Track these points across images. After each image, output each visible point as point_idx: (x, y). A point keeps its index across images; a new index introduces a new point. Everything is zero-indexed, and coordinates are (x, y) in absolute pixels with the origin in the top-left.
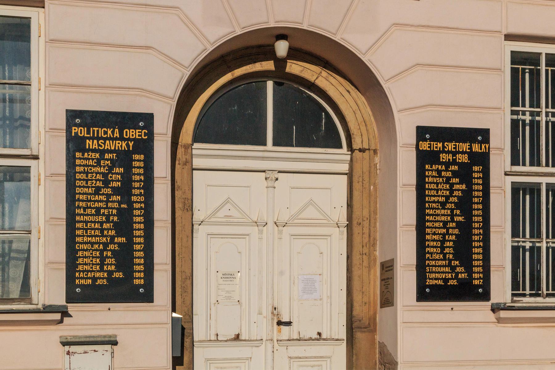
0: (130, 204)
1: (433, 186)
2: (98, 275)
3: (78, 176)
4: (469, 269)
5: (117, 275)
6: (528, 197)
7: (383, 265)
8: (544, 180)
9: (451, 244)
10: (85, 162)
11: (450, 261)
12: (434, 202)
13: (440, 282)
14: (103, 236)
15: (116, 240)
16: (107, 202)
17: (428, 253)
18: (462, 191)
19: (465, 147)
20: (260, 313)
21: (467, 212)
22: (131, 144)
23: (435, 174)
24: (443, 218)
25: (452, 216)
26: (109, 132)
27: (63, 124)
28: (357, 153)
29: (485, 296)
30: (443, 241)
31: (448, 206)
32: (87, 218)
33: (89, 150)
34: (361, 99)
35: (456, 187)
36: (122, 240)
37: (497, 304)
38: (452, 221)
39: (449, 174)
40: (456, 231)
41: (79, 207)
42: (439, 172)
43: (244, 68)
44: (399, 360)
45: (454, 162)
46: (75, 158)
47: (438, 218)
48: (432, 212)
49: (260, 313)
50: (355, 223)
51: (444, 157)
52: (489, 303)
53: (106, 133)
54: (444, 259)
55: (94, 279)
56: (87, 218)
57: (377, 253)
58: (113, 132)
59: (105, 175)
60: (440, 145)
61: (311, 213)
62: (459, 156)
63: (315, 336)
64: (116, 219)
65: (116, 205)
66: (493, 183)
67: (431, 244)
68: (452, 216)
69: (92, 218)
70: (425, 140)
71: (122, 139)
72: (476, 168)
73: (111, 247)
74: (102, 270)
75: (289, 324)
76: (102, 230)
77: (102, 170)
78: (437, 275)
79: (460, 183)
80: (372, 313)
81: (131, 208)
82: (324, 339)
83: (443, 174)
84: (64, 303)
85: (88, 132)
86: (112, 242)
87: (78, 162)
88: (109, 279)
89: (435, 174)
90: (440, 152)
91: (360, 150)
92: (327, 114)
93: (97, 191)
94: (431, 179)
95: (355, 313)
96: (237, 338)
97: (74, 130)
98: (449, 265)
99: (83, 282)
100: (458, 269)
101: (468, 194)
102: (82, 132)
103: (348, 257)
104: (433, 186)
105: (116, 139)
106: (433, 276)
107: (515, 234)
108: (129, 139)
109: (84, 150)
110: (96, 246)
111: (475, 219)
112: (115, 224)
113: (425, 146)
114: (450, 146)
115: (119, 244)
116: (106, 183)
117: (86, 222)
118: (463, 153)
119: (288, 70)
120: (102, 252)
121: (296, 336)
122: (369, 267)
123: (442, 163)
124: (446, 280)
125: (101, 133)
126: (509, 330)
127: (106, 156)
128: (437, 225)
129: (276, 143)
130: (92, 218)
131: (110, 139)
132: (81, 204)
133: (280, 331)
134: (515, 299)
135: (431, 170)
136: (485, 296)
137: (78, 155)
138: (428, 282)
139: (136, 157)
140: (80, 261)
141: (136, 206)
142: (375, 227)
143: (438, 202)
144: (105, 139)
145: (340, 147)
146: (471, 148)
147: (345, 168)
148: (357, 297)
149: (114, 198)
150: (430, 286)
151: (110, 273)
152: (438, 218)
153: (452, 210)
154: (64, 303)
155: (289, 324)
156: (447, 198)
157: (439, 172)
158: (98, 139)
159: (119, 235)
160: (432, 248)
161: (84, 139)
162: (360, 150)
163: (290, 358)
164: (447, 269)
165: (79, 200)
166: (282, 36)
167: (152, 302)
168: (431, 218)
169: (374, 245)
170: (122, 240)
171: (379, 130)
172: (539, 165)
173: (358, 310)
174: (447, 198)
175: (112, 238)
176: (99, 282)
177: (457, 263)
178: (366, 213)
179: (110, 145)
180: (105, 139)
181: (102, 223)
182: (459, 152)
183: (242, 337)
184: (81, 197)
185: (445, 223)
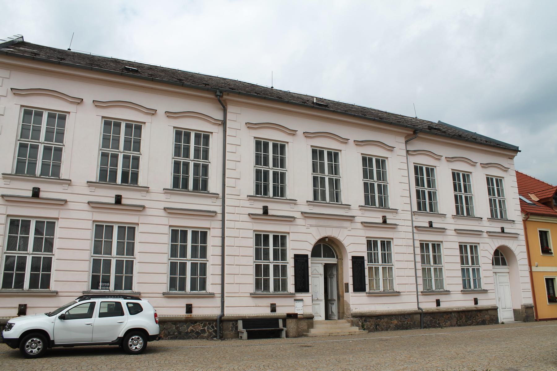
19: (360, 260)
149: (302, 271)
172: (372, 263)
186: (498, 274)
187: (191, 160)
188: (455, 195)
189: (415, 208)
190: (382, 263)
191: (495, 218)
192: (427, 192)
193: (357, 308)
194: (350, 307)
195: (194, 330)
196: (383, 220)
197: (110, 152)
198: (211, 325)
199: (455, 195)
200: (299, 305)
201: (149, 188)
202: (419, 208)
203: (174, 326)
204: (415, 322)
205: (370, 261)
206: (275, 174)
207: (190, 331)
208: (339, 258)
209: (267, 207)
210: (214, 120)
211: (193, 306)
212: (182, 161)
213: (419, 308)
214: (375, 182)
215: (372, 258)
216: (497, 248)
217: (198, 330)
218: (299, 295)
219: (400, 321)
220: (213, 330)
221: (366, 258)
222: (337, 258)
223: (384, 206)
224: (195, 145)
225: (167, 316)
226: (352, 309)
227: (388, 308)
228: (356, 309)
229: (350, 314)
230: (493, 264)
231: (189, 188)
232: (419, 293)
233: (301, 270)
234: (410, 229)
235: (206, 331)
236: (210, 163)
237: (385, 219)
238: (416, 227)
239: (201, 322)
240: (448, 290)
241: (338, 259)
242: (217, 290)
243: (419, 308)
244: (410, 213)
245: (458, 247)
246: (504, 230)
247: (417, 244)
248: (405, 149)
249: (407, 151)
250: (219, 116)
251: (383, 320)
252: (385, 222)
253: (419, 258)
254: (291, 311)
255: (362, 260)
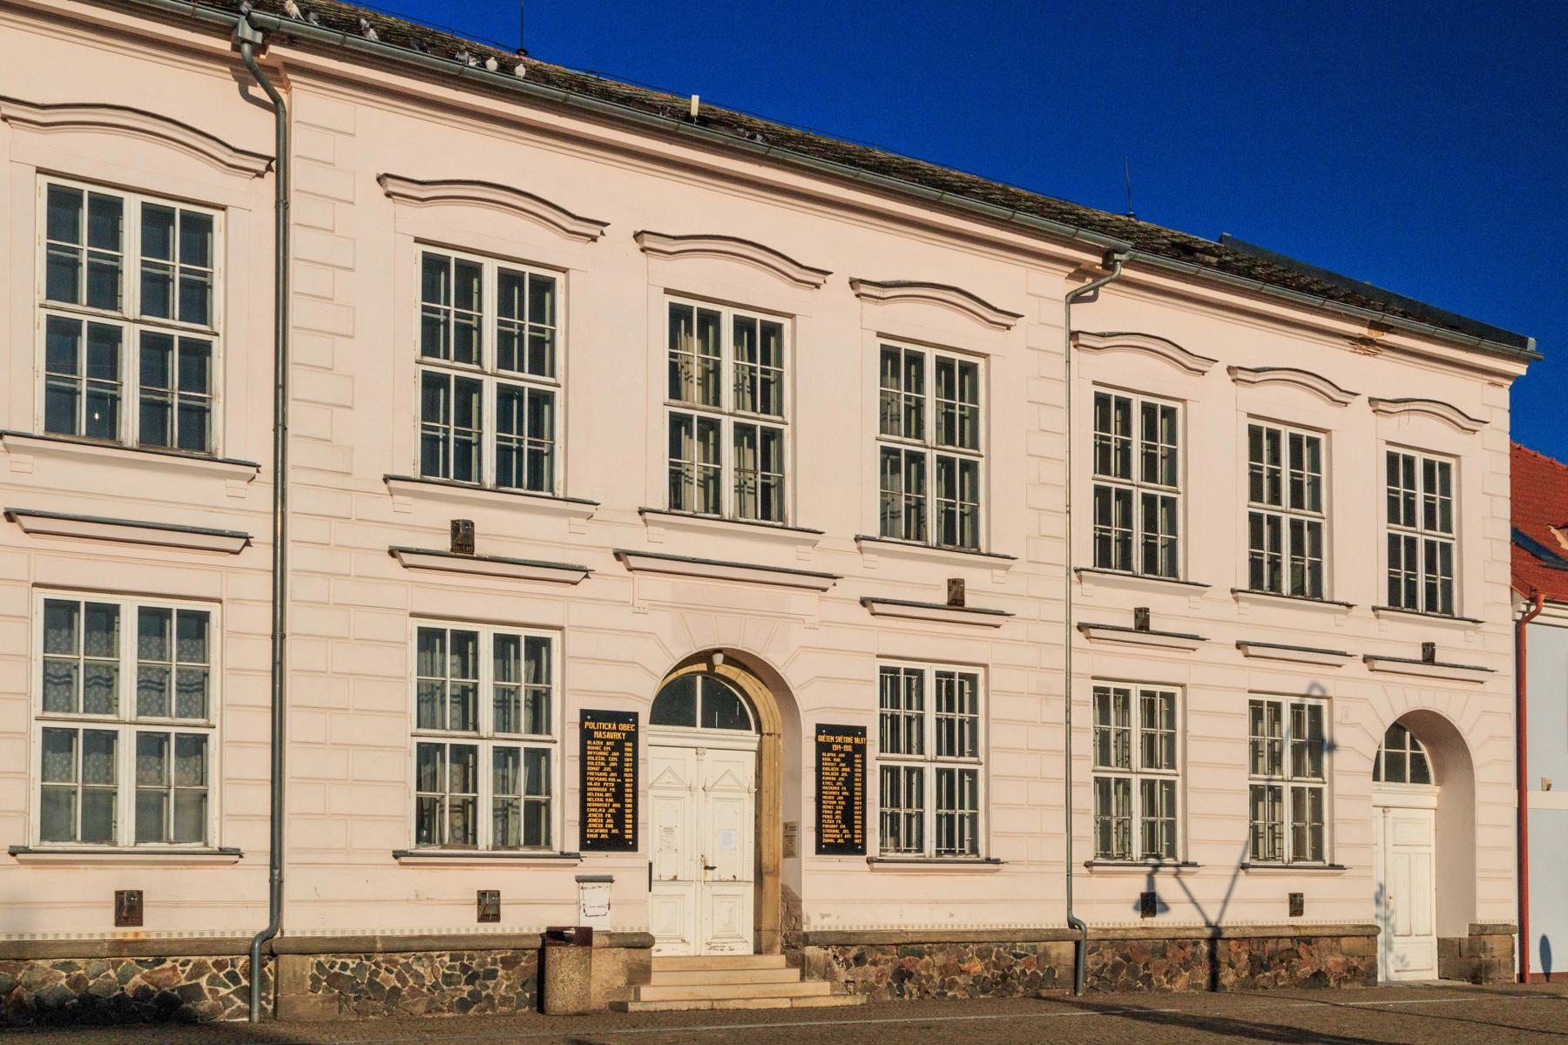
0: (623, 779)
1: (828, 769)
2: (601, 831)
3: (589, 758)
4: (852, 832)
5: (613, 831)
6: (889, 774)
7: (786, 826)
8: (453, 373)
9: (840, 812)
10: (593, 748)
11: (839, 825)
12: (828, 781)
13: (832, 841)
14: (605, 802)
15: (614, 805)
16: (608, 777)
17: (824, 818)
18: (848, 773)
19: (849, 739)
20: (692, 860)
21: (851, 790)
22: (624, 735)
23: (829, 759)
24: (834, 793)
25: (841, 791)
26: (610, 725)
27: (578, 720)
28: (765, 737)
29: (863, 852)
30: (834, 810)
31: (838, 784)
32: (595, 789)
33: (596, 739)
34: (770, 695)
35: (843, 770)
36: (618, 805)
37: (872, 858)
38: (841, 795)
39: (838, 760)
40: (843, 803)
41: (589, 781)
42: (832, 758)
43: (686, 668)
44: (804, 897)
45: (842, 751)
46: (586, 745)
47: (831, 793)
48: (826, 788)
49: (692, 860)
50: (764, 790)
51: (836, 747)
52: (865, 857)
53: (607, 726)
54: (835, 824)
55: (599, 834)
56: (595, 789)
57: (780, 815)
58: (612, 726)
59: (606, 757)
60: (832, 738)
61: (728, 780)
62: (845, 746)
63: (732, 879)
64: (613, 790)
65: (614, 780)
66: (868, 767)
67: (826, 812)
68: (841, 791)
69: (598, 789)
70: (822, 734)
71: (618, 731)
72: (857, 756)
73: (610, 810)
74: (604, 828)
75: (713, 868)
76: (604, 798)
77: (605, 754)
78: (830, 836)
79: (847, 767)
80: (776, 861)
81: (624, 782)
82: (739, 881)
83: (834, 759)
84: (578, 851)
85: (596, 726)
86: (611, 807)
87: (589, 748)
88: (609, 834)
89: (829, 759)
90: (832, 743)
91: (768, 734)
92: (741, 703)
93: (601, 769)
94: (826, 764)
95: (763, 861)
96: (675, 878)
97: (587, 724)
98: (839, 828)
99: (592, 836)
100: (845, 831)
101: (851, 775)
102: (591, 725)
103: (756, 817)
104: (828, 769)
105: (614, 731)
106: (827, 836)
107: (882, 805)
108: (623, 731)
109: (593, 739)
110: (600, 810)
111: (856, 794)
112: (613, 793)
113: (822, 738)
114: (839, 739)
115: (616, 809)
116: (607, 763)
117: (594, 792)
118: (848, 744)
119: (705, 665)
120: (604, 814)
121: (717, 879)
122: (774, 825)
123: (834, 752)
124: (836, 839)
125: (604, 727)
126: (879, 877)
127: (608, 743)
128: (830, 797)
129: (704, 725)
130: (598, 789)
131: (610, 731)
132: (591, 779)
133: (706, 874)
134: (883, 854)
135: (826, 756)
136: (863, 852)
137: (589, 742)
138: (825, 841)
139: (627, 744)
140: (590, 820)
141: (627, 780)
142: (779, 794)
143: (831, 781)
144: (607, 731)
145: (751, 729)
146: (853, 741)
147: (755, 746)
148: (765, 850)
149: (612, 774)
150: (825, 844)
151: (610, 830)
152: (831, 793)
153: (841, 787)
154: (578, 851)
155: (713, 868)
156: (837, 777)
157: (832, 758)
158: (602, 730)
159: (616, 802)
160: (827, 816)
161: (593, 731)
162: (768, 734)
163: (713, 895)
164: (837, 831)
165: (589, 776)
166: (719, 651)
167: (637, 851)
168: (826, 793)
169: (778, 808)
170: (618, 805)
171: (782, 719)
172: (898, 752)
173: (765, 860)
174: (837, 777)
175: (611, 803)
176: (602, 836)
177: (844, 826)
178: (772, 784)
179: (610, 735)
180: (607, 731)
181: (604, 793)
182: (845, 744)
183: (679, 878)
184: (591, 774)
185: (836, 796)
186: (1393, 813)
187: (127, 320)
188: (1390, 535)
189: (1085, 554)
190: (939, 753)
191: (1405, 609)
192: (1423, 541)
193: (829, 915)
194: (800, 908)
195: (151, 987)
196: (952, 593)
197: (177, 334)
198: (229, 969)
199: (1390, 535)
200: (596, 895)
201: (259, 466)
202: (1103, 559)
203: (64, 974)
204: (1052, 971)
205: (892, 741)
206: (507, 395)
207: (136, 993)
208: (765, 729)
209: (469, 525)
210: (230, 152)
211: (1305, 898)
212: (86, 319)
213: (1072, 923)
214: (927, 447)
215: (896, 733)
216: (1399, 719)
217: (167, 989)
218: (598, 862)
219: (996, 966)
220: (233, 988)
221: (873, 736)
222: (759, 729)
223: (958, 542)
224: (142, 255)
225: (155, 937)
226: (808, 918)
227: (952, 915)
228: (823, 916)
229: (801, 933)
230: (1376, 777)
231: (929, 539)
232: (1078, 869)
233: (609, 769)
234: (1059, 635)
235: (206, 991)
236: (217, 334)
237: (956, 592)
238: (1081, 627)
239: (182, 959)
240: (1341, 864)
241: (762, 734)
242: (257, 839)
243: (1072, 923)
244: (1063, 571)
245: (1246, 709)
246: (1147, 619)
247: (1084, 692)
248: (1063, 324)
249: (1074, 335)
250: (256, 130)
251: (927, 957)
252: (956, 600)
253: (1085, 744)
254: (566, 919)
255: (857, 740)
